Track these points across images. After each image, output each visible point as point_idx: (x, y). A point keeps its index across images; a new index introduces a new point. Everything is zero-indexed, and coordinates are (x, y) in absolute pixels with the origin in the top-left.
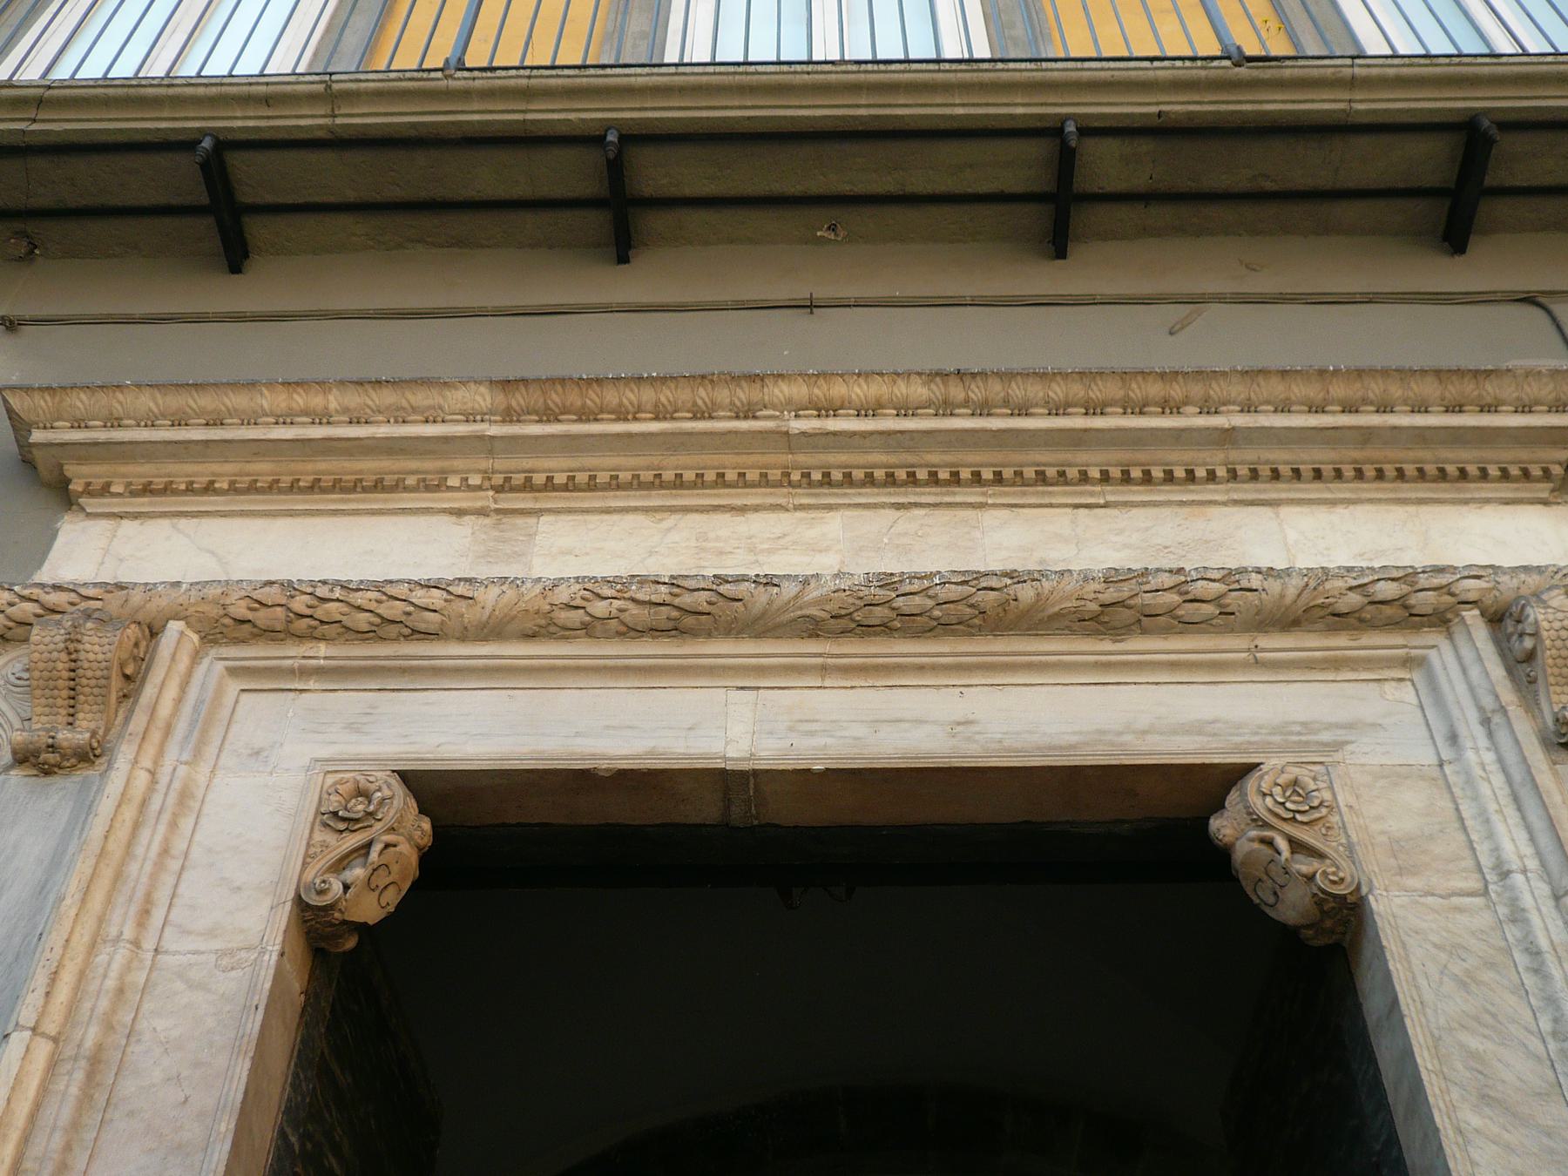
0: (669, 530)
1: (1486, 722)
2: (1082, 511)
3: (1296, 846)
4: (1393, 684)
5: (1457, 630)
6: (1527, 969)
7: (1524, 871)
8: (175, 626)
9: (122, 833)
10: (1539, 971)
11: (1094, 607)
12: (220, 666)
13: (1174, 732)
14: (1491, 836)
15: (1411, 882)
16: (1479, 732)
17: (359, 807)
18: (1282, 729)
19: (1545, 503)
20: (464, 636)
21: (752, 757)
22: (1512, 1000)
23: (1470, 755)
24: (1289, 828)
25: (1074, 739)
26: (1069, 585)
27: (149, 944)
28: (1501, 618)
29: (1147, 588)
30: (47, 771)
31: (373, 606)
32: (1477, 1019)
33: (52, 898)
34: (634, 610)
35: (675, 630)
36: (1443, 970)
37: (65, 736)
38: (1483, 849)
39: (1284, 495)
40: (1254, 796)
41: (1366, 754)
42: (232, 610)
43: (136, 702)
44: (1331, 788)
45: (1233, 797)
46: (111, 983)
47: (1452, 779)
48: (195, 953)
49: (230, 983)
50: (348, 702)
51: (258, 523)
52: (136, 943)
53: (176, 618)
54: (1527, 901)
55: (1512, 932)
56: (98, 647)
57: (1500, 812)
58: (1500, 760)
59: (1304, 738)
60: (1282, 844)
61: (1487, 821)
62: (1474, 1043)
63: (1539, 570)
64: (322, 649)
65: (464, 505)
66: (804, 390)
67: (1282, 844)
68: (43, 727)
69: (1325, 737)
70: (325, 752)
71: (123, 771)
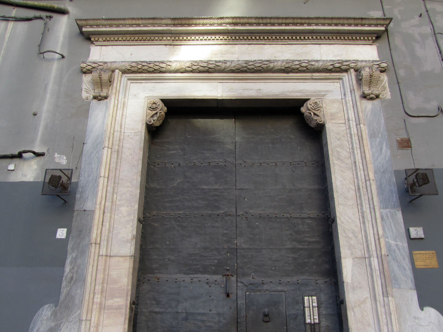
1: (351, 92)
3: (315, 114)
5: (349, 72)
8: (117, 71)
9: (115, 112)
10: (351, 138)
11: (284, 68)
12: (126, 78)
13: (296, 92)
14: (348, 113)
16: (349, 93)
17: (154, 106)
18: (314, 92)
19: (371, 45)
20: (170, 72)
21: (222, 96)
22: (346, 142)
24: (314, 111)
25: (278, 93)
26: (279, 63)
27: (123, 131)
28: (357, 70)
30: (100, 100)
31: (153, 67)
32: (340, 146)
33: (105, 124)
34: (201, 68)
35: (207, 72)
36: (336, 137)
37: (102, 94)
38: (346, 115)
39: (322, 43)
40: (309, 104)
41: (329, 97)
42: (127, 68)
43: (113, 86)
45: (305, 105)
46: (118, 139)
47: (343, 102)
49: (137, 138)
50: (150, 85)
52: (121, 131)
53: (117, 69)
56: (105, 77)
58: (352, 99)
60: (312, 114)
62: (338, 150)
63: (366, 61)
64: (144, 75)
65: (167, 43)
66: (231, 20)
67: (312, 114)
68: (97, 92)
69: (323, 93)
70: (148, 95)
71: (112, 100)
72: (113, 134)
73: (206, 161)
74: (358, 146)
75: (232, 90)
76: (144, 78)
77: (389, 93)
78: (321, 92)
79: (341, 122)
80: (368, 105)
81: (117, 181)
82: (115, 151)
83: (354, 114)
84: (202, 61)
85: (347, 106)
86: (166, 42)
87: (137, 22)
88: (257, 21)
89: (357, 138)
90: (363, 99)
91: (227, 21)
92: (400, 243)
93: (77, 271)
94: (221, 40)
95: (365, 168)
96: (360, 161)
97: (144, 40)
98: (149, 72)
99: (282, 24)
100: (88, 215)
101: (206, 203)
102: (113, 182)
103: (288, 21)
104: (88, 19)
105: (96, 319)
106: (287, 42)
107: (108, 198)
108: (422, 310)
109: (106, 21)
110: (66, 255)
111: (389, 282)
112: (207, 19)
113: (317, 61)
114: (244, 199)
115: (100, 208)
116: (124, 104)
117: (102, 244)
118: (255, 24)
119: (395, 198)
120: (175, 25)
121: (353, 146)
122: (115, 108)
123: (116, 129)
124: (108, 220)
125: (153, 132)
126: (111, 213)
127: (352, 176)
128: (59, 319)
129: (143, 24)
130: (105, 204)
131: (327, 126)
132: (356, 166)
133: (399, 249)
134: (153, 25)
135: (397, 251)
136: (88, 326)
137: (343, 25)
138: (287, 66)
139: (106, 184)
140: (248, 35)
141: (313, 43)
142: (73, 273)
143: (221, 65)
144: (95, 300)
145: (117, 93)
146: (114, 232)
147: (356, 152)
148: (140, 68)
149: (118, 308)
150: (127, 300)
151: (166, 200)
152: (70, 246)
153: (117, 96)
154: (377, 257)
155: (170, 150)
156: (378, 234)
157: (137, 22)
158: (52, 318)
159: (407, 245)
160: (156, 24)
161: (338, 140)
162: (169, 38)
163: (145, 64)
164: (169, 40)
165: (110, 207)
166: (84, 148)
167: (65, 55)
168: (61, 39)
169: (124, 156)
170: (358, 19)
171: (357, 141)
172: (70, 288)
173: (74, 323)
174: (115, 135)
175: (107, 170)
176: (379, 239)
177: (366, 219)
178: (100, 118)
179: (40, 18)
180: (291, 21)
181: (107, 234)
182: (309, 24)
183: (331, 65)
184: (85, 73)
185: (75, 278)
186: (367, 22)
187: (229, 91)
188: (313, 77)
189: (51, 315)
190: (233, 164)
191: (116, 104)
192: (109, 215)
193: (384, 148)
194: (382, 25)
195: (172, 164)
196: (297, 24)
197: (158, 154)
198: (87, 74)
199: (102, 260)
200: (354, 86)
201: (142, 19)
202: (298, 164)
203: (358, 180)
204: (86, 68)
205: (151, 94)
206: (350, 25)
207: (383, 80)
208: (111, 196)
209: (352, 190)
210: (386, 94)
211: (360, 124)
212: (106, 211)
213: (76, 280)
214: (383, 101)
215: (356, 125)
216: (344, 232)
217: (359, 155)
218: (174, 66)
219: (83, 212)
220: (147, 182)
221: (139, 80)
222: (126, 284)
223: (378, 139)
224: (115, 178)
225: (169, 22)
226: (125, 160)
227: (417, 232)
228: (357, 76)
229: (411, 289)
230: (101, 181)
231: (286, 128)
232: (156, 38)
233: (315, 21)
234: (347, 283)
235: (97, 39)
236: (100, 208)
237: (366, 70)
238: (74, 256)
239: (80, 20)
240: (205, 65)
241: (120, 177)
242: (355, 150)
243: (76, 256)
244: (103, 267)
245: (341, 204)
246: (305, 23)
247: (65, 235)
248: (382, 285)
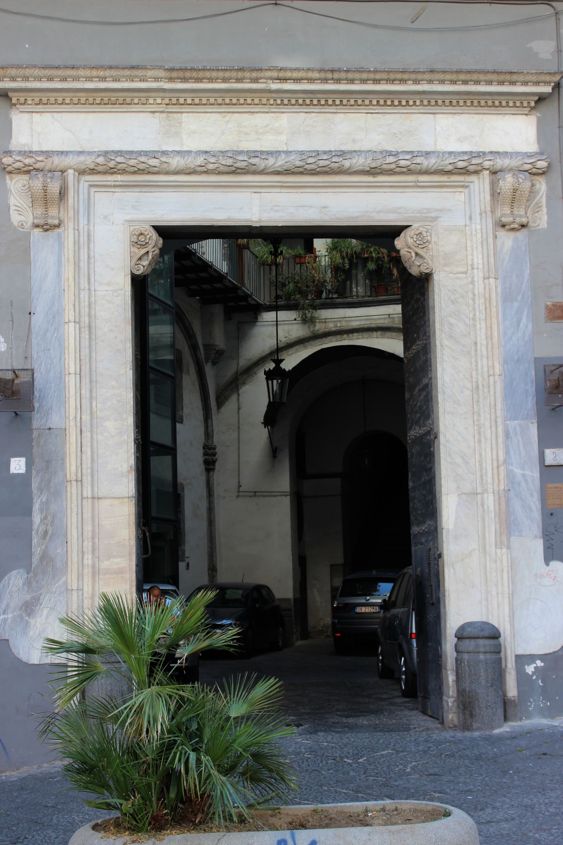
0: (228, 122)
1: (481, 214)
2: (369, 114)
3: (417, 254)
4: (458, 193)
5: (481, 176)
6: (471, 299)
7: (478, 269)
8: (71, 172)
15: (447, 269)
16: (478, 217)
19: (526, 115)
20: (167, 173)
21: (260, 221)
23: (473, 225)
27: (92, 289)
29: (385, 162)
35: (233, 173)
39: (438, 111)
44: (431, 235)
45: (402, 235)
48: (106, 291)
50: (131, 196)
51: (83, 115)
52: (89, 289)
54: (476, 279)
55: (471, 286)
57: (476, 248)
58: (481, 229)
59: (427, 215)
61: (472, 250)
62: (452, 321)
65: (155, 110)
67: (413, 254)
69: (433, 215)
70: (128, 217)
71: (69, 233)
76: (121, 183)
77: (545, 217)
80: (507, 240)
81: (94, 379)
86: (155, 108)
88: (322, 75)
92: (528, 473)
93: (52, 522)
96: (484, 342)
100: (56, 436)
105: (90, 588)
108: (547, 564)
110: (31, 499)
111: (508, 526)
113: (427, 154)
117: (84, 480)
119: (530, 403)
124: (89, 444)
126: (92, 432)
128: (35, 589)
131: (436, 277)
133: (526, 481)
135: (523, 484)
136: (81, 597)
137: (477, 82)
138: (373, 165)
142: (47, 525)
143: (257, 164)
144: (85, 562)
146: (100, 461)
148: (112, 166)
149: (120, 571)
150: (131, 560)
152: (35, 485)
154: (493, 492)
156: (498, 461)
157: (102, 73)
158: (26, 588)
159: (538, 475)
161: (453, 303)
162: (159, 101)
165: (89, 422)
166: (32, 322)
172: (46, 547)
173: (59, 594)
176: (498, 467)
177: (482, 437)
180: (384, 76)
181: (89, 465)
185: (50, 532)
186: (521, 78)
188: (418, 184)
189: (23, 585)
192: (89, 435)
193: (524, 320)
194: (547, 83)
196: (395, 80)
199: (87, 505)
204: (13, 165)
206: (490, 83)
208: (88, 405)
209: (468, 389)
210: (540, 219)
212: (84, 429)
213: (53, 535)
216: (450, 455)
219: (47, 431)
222: (127, 538)
223: (516, 304)
224: (90, 374)
226: (102, 341)
227: (553, 456)
229: (536, 537)
234: (448, 530)
237: (508, 180)
238: (44, 500)
243: (47, 500)
244: (90, 515)
245: (449, 413)
247: (25, 469)
248: (496, 533)
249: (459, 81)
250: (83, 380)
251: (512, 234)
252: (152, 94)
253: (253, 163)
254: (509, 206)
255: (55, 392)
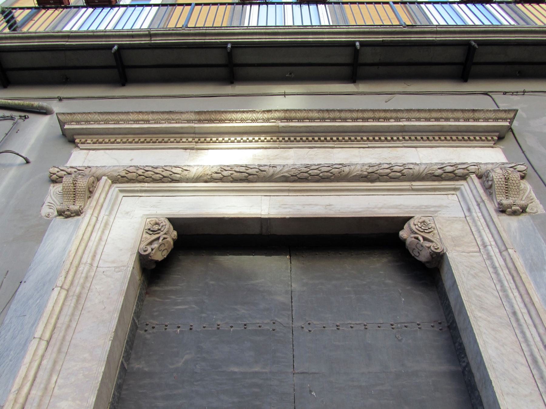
1: (478, 205)
3: (425, 239)
5: (469, 179)
8: (104, 178)
10: (496, 273)
11: (366, 173)
14: (481, 236)
16: (477, 208)
17: (156, 227)
19: (492, 147)
20: (188, 180)
25: (360, 210)
26: (358, 167)
27: (95, 265)
30: (68, 217)
31: (161, 172)
33: (67, 251)
34: (235, 174)
38: (479, 240)
39: (418, 145)
41: (444, 214)
45: (406, 226)
46: (84, 275)
47: (469, 221)
52: (91, 265)
53: (104, 175)
58: (483, 215)
60: (421, 239)
62: (478, 293)
63: (492, 164)
65: (187, 146)
66: (283, 114)
67: (421, 239)
69: (432, 209)
70: (148, 213)
72: (77, 267)
73: (240, 322)
74: (513, 286)
75: (284, 206)
77: (541, 206)
78: (429, 208)
79: (471, 249)
81: (65, 349)
82: (73, 296)
83: (493, 236)
84: (237, 166)
85: (476, 226)
87: (146, 117)
88: (321, 115)
89: (506, 271)
90: (501, 214)
91: (277, 115)
94: (268, 141)
95: (537, 321)
96: (524, 311)
97: (153, 142)
98: (155, 181)
99: (357, 119)
101: (236, 400)
102: (56, 350)
103: (366, 115)
104: (74, 113)
106: (367, 144)
107: (38, 380)
109: (101, 116)
112: (247, 112)
114: (311, 391)
115: (16, 401)
116: (106, 224)
118: (318, 119)
120: (200, 121)
121: (502, 286)
122: (90, 228)
123: (84, 260)
125: (152, 272)
127: (514, 338)
129: (153, 120)
130: (29, 393)
132: (517, 320)
134: (169, 121)
138: (370, 170)
139: (40, 352)
140: (308, 134)
141: (405, 145)
143: (267, 170)
145: (98, 208)
147: (511, 295)
148: (141, 173)
151: (159, 394)
153: (97, 212)
155: (177, 304)
157: (146, 117)
160: (173, 120)
161: (474, 277)
162: (190, 140)
163: (150, 169)
164: (191, 142)
165: (37, 400)
166: (20, 290)
167: (30, 159)
168: (32, 141)
169: (88, 304)
170: (468, 111)
171: (509, 277)
174: (81, 269)
175: (50, 327)
178: (62, 241)
179: (12, 118)
180: (371, 115)
182: (397, 119)
183: (439, 169)
184: (54, 182)
187: (280, 207)
190: (289, 327)
191: (92, 223)
194: (505, 119)
195: (179, 327)
197: (155, 310)
198: (57, 184)
200: (482, 196)
201: (153, 112)
202: (406, 327)
203: (528, 345)
204: (57, 174)
205: (153, 211)
206: (457, 120)
207: (525, 190)
209: (522, 364)
211: (507, 249)
214: (535, 216)
215: (501, 253)
217: (519, 299)
218: (194, 172)
220: (127, 356)
221: (137, 191)
225: (193, 117)
226: (89, 312)
228: (483, 185)
230: (34, 344)
231: (376, 272)
232: (172, 140)
233: (405, 115)
235: (83, 140)
236: (16, 401)
239: (63, 114)
240: (243, 169)
241: (73, 342)
242: (509, 291)
245: (508, 394)
246: (391, 118)
249: (432, 119)
250: (50, 349)
251: (514, 219)
252: (185, 135)
253: (263, 169)
254: (504, 196)
255: (11, 361)
